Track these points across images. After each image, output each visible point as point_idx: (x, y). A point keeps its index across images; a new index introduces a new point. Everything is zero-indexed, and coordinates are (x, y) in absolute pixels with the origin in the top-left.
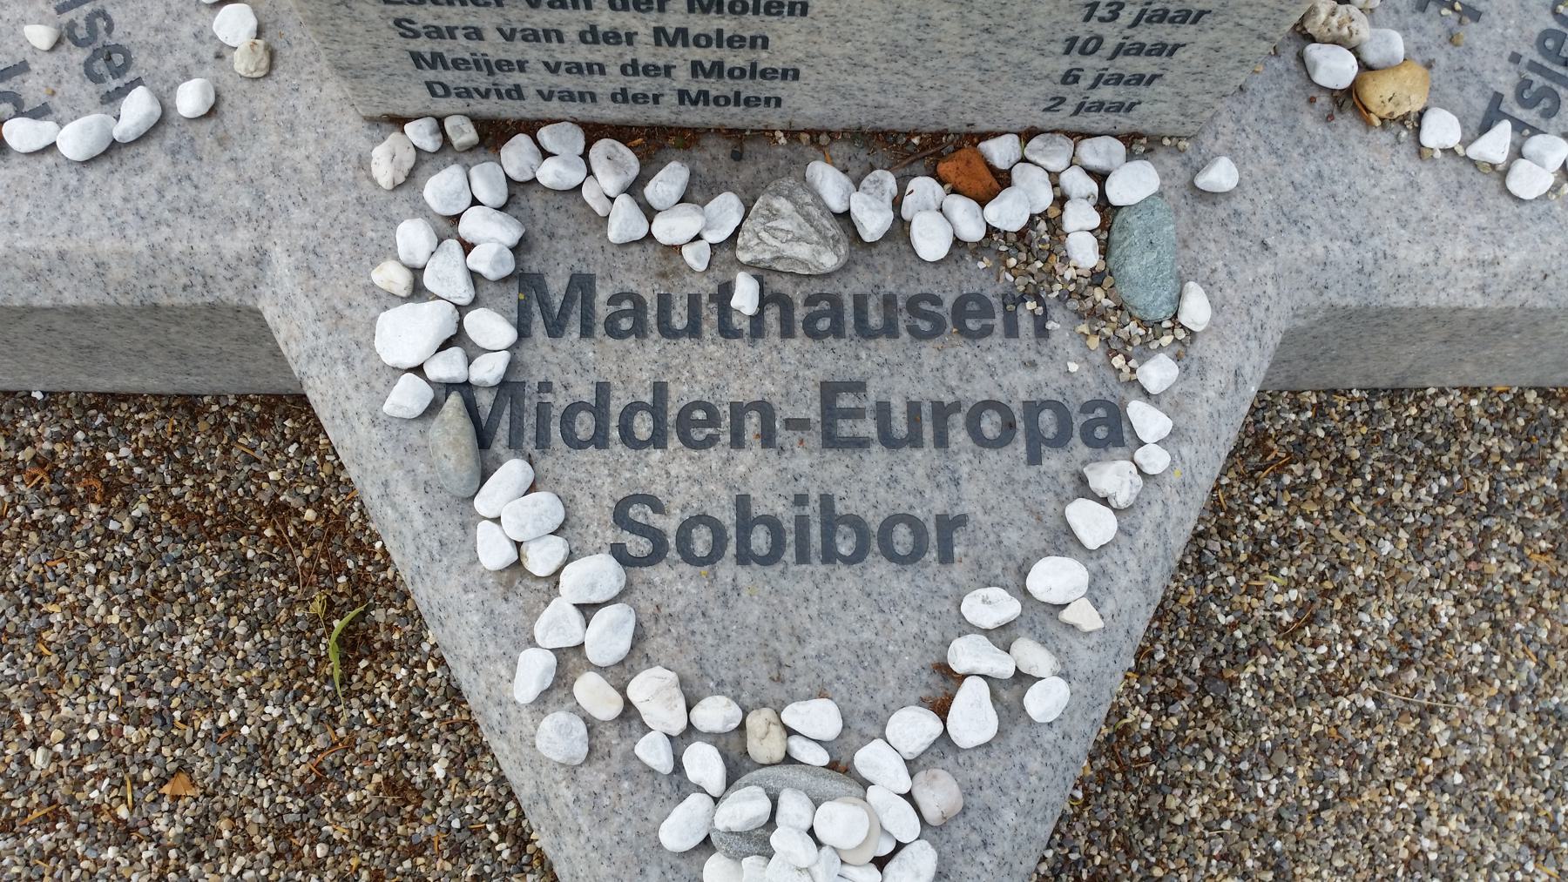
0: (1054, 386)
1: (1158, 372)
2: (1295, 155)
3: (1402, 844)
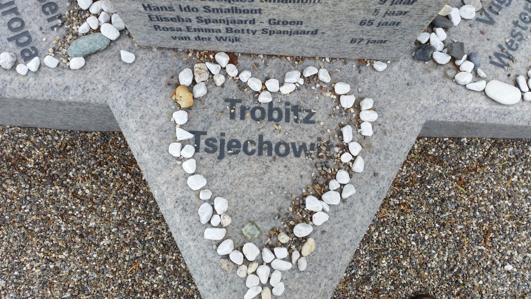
0: (37, 37)
1: (50, 61)
2: (150, 78)
3: (25, 258)
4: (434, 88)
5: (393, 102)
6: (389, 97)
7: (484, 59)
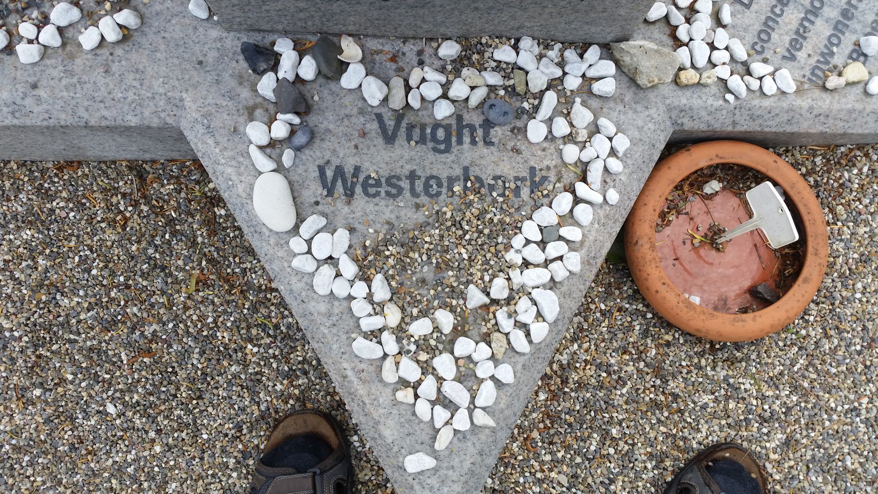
4: (218, 103)
5: (158, 55)
6: (162, 47)
7: (318, 154)
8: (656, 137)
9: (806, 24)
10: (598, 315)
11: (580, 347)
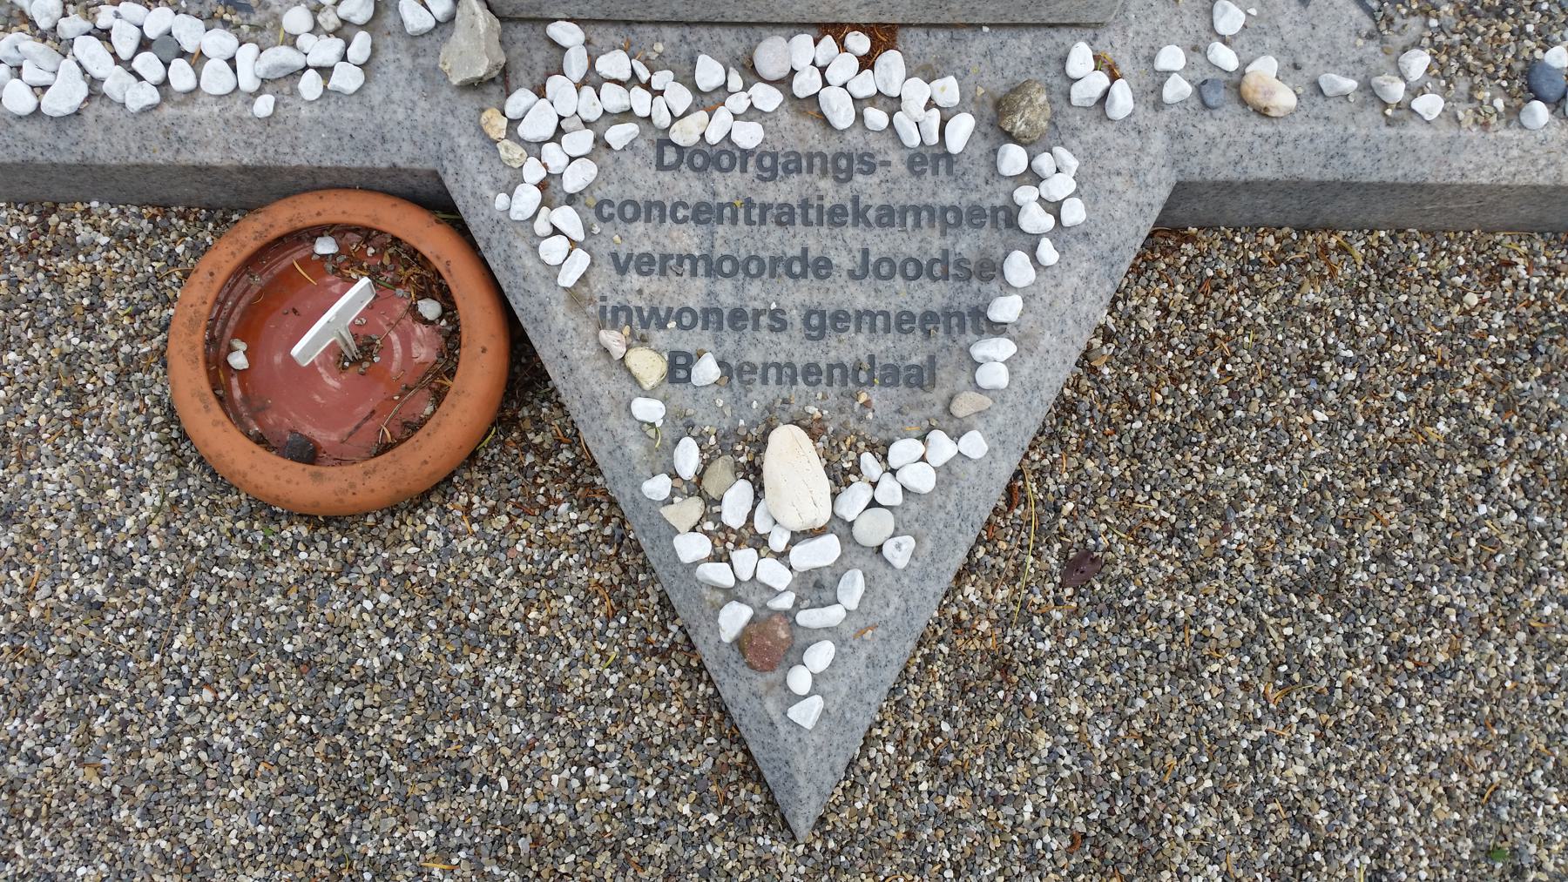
8: (397, 135)
9: (687, 265)
10: (165, 249)
11: (108, 248)
